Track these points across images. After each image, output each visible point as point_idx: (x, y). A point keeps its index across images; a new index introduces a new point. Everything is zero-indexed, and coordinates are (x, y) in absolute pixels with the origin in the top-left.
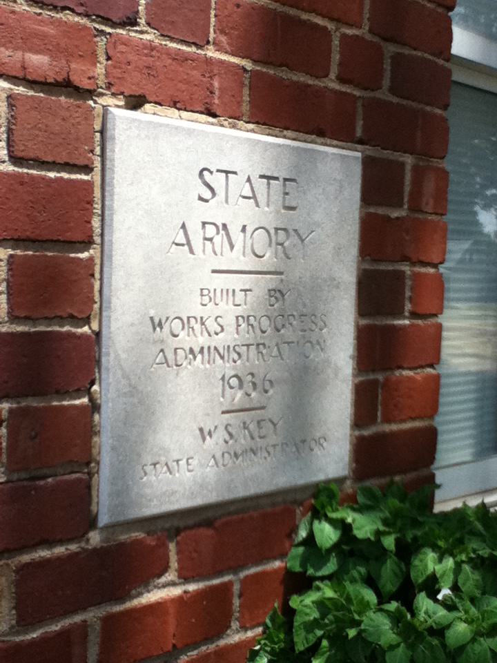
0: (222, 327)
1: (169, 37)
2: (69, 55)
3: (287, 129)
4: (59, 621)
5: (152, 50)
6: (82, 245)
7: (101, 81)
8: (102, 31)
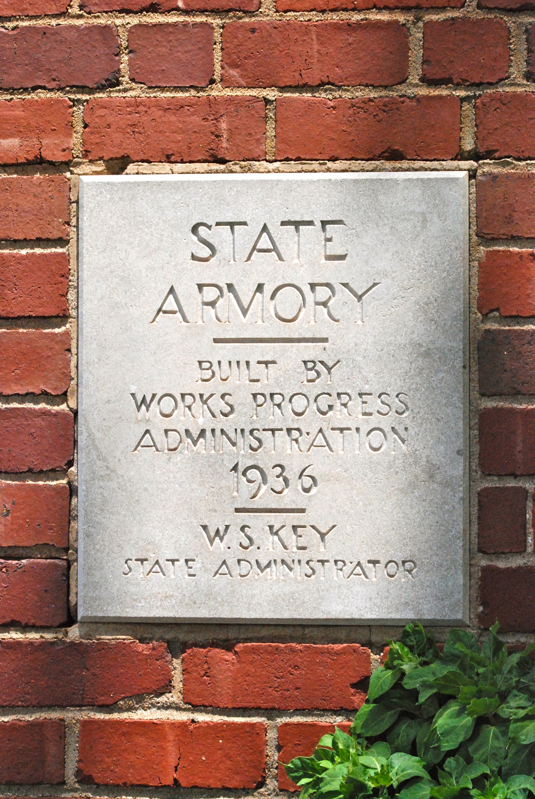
0: (231, 406)
1: (159, 87)
2: (41, 132)
3: (333, 159)
4: (33, 713)
5: (138, 106)
6: (59, 320)
7: (78, 150)
8: (78, 100)
